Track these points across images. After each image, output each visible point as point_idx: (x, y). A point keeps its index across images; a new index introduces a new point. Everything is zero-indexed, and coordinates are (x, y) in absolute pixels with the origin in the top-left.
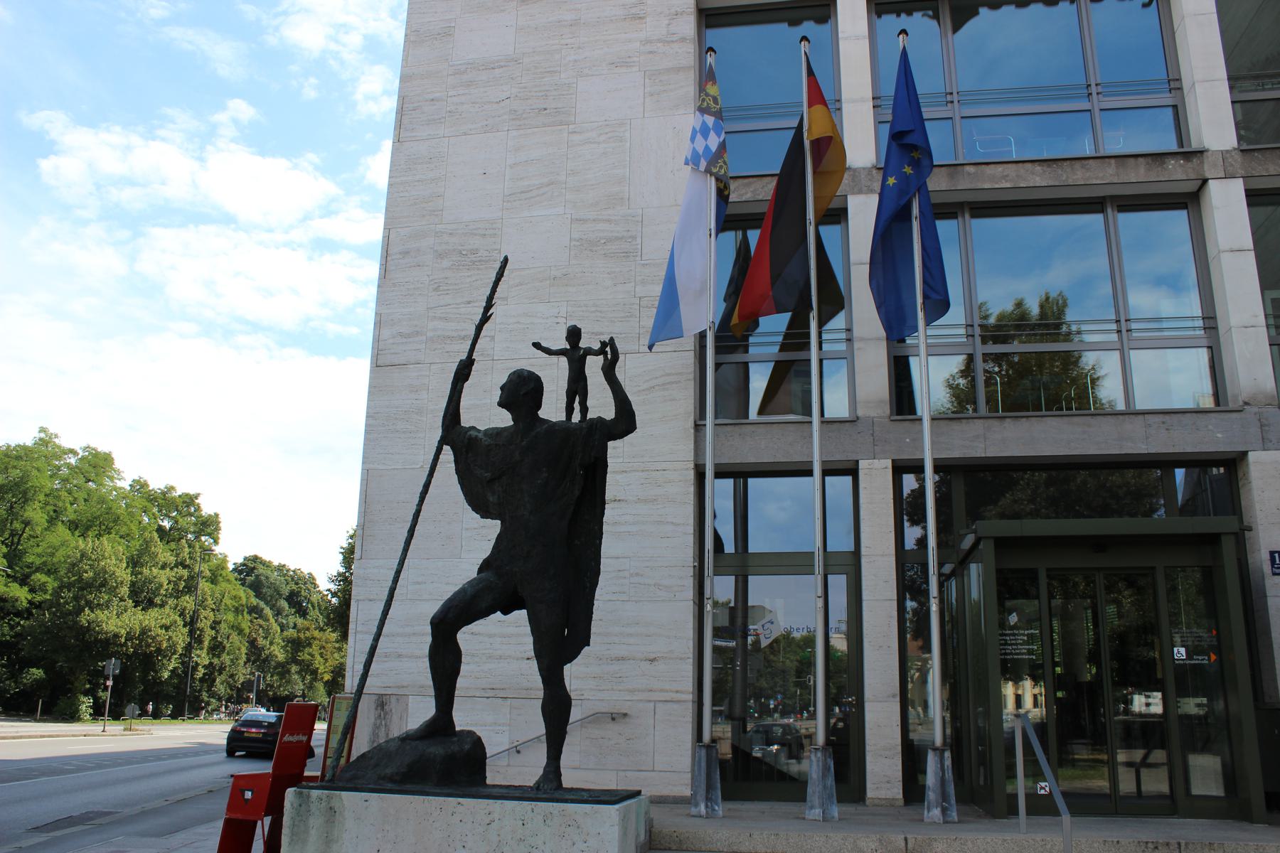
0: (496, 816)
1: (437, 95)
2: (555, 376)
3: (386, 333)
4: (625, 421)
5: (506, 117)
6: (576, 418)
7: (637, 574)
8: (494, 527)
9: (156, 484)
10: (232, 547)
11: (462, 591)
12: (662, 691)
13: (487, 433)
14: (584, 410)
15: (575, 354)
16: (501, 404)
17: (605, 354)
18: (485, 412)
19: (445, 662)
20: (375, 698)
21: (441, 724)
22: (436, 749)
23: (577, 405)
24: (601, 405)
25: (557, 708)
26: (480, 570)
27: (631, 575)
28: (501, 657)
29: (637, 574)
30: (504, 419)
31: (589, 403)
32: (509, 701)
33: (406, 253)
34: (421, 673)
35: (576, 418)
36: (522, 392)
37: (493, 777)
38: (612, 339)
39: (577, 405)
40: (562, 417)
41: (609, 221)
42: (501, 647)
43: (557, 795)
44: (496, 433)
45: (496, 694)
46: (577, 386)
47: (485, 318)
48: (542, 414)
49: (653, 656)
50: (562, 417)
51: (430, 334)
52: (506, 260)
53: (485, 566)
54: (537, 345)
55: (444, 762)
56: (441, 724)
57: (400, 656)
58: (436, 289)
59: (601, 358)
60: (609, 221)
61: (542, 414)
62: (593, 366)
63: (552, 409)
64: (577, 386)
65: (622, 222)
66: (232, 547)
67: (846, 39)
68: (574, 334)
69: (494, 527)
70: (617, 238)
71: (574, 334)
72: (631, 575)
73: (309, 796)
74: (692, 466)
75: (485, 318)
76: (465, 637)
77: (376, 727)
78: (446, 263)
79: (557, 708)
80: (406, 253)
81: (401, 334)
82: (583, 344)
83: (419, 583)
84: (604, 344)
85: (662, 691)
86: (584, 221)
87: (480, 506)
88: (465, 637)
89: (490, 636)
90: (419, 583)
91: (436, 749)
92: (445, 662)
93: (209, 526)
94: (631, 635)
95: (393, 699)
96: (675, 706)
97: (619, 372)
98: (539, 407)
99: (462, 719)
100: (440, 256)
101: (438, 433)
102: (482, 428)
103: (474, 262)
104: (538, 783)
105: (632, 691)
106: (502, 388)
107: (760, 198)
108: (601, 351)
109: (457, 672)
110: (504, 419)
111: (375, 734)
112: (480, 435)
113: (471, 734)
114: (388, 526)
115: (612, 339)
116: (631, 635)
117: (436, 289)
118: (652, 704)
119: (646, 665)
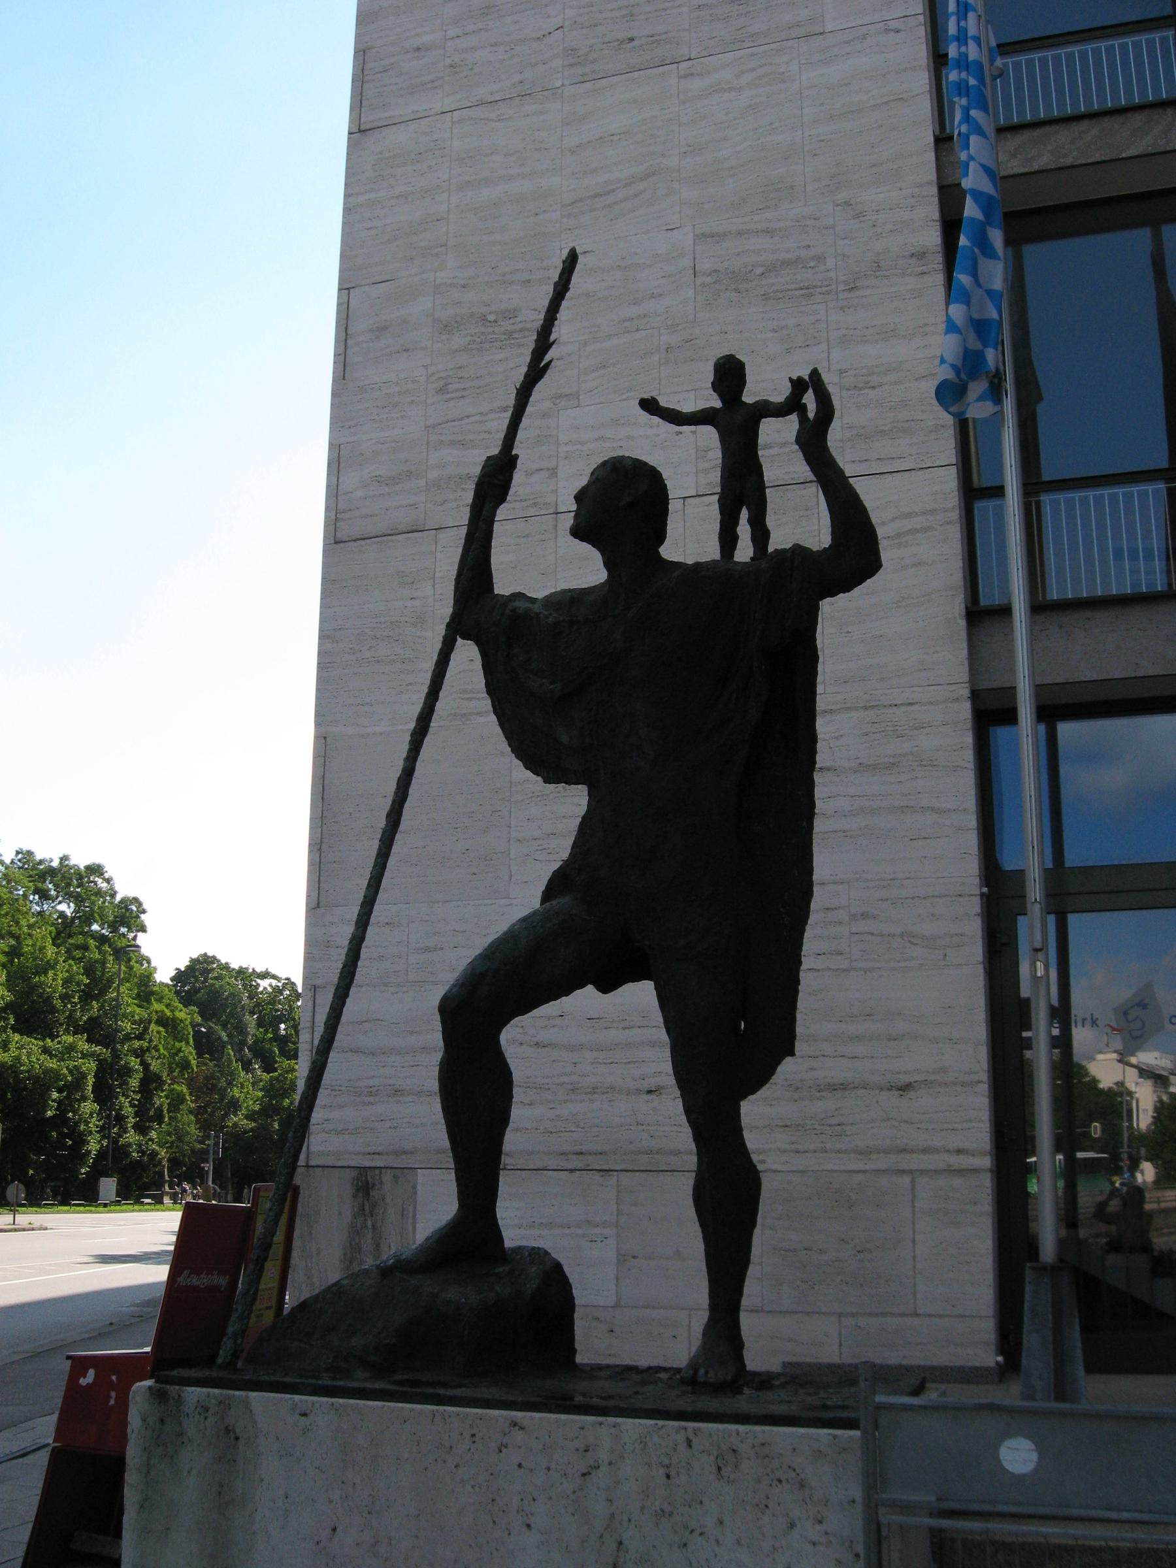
0: (603, 1455)
1: (426, 39)
2: (689, 465)
3: (350, 480)
4: (854, 552)
5: (558, 63)
6: (744, 552)
7: (865, 916)
8: (573, 802)
9: (48, 852)
10: (165, 952)
11: (509, 939)
12: (926, 1150)
13: (549, 601)
14: (761, 535)
15: (734, 416)
16: (578, 532)
17: (802, 410)
18: (548, 560)
19: (476, 1094)
20: (350, 1175)
21: (474, 1233)
22: (460, 1294)
23: (744, 530)
24: (799, 520)
25: (728, 1197)
26: (549, 894)
27: (853, 917)
28: (594, 1090)
29: (865, 916)
30: (585, 568)
31: (770, 521)
32: (613, 1180)
33: (381, 330)
34: (423, 1122)
35: (744, 552)
36: (621, 506)
37: (592, 1344)
38: (815, 373)
39: (744, 530)
40: (710, 551)
41: (768, 232)
42: (596, 1056)
43: (743, 1402)
44: (570, 602)
45: (589, 1164)
46: (742, 488)
47: (536, 372)
48: (669, 551)
49: (905, 1079)
50: (710, 551)
51: (433, 475)
52: (572, 259)
53: (557, 885)
54: (650, 406)
55: (482, 1326)
56: (474, 1233)
57: (397, 1092)
58: (441, 391)
59: (794, 418)
60: (768, 232)
61: (669, 551)
62: (777, 439)
63: (691, 535)
64: (742, 488)
65: (794, 212)
66: (165, 952)
67: (517, 1130)
68: (729, 374)
69: (573, 802)
70: (787, 263)
71: (729, 374)
72: (853, 917)
73: (179, 1401)
74: (966, 693)
75: (536, 372)
76: (524, 1040)
77: (356, 1232)
78: (457, 341)
79: (728, 1197)
80: (381, 330)
81: (378, 480)
82: (748, 398)
83: (427, 950)
84: (799, 386)
85: (926, 1150)
86: (722, 236)
87: (543, 756)
88: (524, 1040)
89: (573, 1048)
90: (427, 950)
91: (460, 1294)
92: (476, 1094)
93: (129, 915)
94: (856, 1039)
95: (387, 1177)
96: (956, 1181)
97: (835, 437)
98: (661, 537)
99: (519, 1220)
100: (448, 328)
101: (446, 609)
102: (539, 595)
103: (510, 334)
104: (694, 1365)
105: (865, 1153)
106: (578, 498)
107: (1069, 161)
108: (793, 405)
109: (502, 1119)
110: (585, 568)
111: (352, 1250)
112: (536, 608)
113: (538, 1255)
114: (362, 848)
115: (815, 373)
116: (856, 1039)
117: (441, 391)
118: (907, 1179)
119: (890, 1100)
